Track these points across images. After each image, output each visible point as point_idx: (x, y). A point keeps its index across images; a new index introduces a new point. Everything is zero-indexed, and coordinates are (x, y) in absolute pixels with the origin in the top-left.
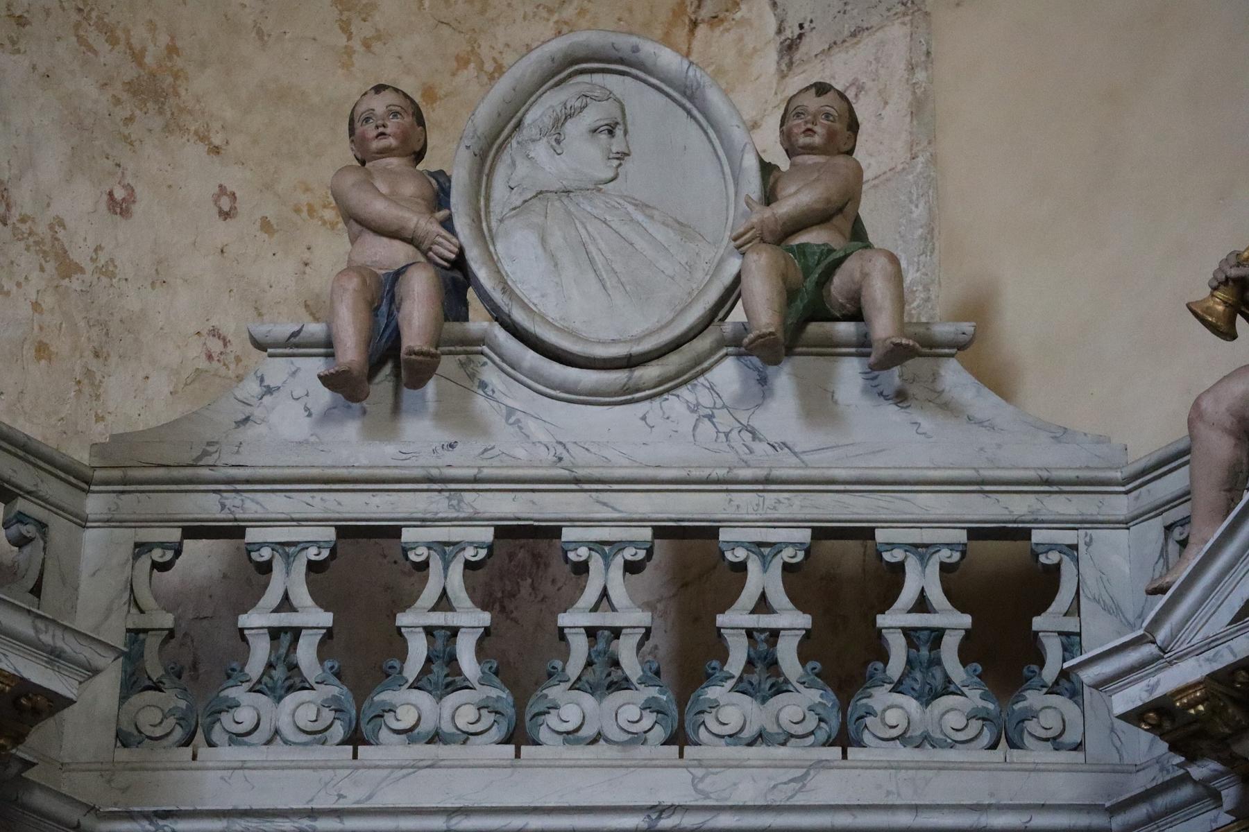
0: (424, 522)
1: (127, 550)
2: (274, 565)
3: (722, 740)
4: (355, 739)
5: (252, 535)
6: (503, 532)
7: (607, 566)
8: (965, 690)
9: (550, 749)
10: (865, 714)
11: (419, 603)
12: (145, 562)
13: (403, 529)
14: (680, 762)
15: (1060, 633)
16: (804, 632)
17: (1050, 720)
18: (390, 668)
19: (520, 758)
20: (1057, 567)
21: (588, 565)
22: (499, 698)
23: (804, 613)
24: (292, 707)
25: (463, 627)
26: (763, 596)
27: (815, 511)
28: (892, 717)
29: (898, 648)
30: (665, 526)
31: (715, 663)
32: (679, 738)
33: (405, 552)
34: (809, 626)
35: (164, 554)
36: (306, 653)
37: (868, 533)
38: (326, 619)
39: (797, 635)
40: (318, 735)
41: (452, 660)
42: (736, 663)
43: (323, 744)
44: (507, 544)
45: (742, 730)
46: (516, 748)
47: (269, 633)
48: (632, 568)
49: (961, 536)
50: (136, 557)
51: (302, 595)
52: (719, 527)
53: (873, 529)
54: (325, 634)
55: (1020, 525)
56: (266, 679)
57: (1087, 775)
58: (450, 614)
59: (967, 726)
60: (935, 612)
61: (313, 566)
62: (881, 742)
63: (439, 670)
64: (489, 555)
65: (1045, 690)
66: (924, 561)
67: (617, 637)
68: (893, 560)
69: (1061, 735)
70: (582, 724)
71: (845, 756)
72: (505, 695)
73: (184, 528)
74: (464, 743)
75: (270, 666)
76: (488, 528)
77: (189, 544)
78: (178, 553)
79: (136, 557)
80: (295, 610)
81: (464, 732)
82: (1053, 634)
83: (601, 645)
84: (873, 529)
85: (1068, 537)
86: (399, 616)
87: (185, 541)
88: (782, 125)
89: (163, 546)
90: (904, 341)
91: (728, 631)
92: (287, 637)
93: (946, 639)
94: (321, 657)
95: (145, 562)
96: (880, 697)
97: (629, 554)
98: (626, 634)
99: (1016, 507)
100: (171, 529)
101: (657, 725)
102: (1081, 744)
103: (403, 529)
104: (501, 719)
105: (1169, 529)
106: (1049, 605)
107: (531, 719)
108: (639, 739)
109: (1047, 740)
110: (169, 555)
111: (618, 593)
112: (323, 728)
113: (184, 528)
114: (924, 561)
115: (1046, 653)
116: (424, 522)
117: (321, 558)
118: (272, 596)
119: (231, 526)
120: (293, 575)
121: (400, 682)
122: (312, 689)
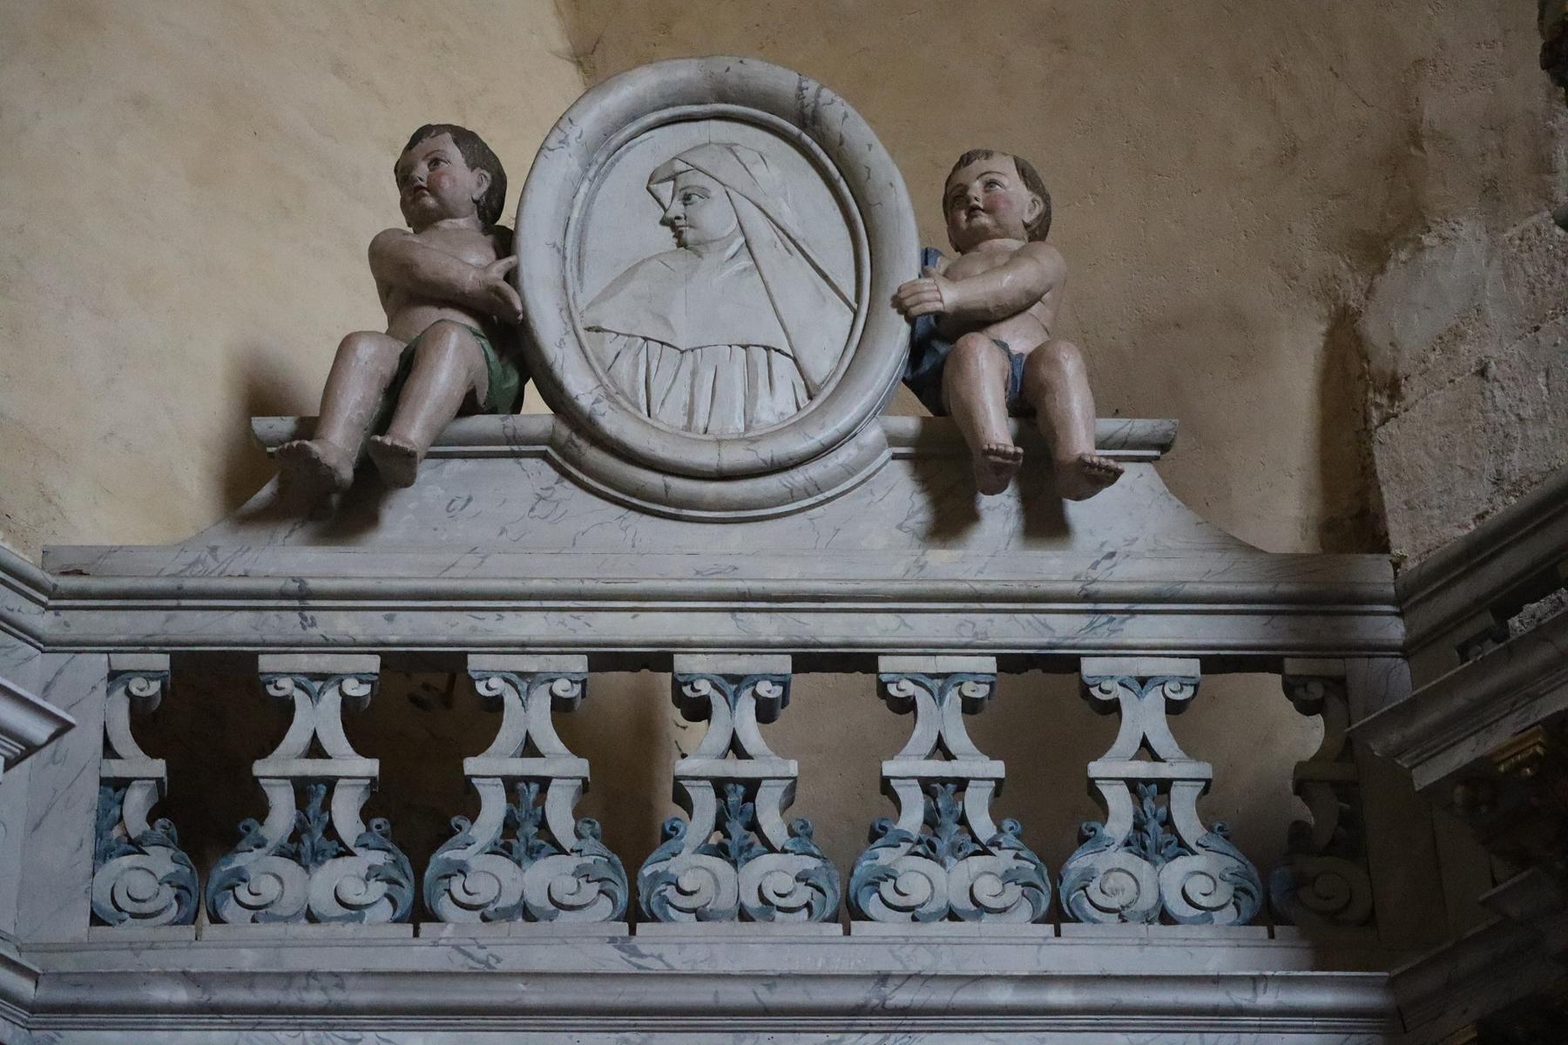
7: (732, 708)
14: (1057, 940)
19: (849, 934)
24: (1143, 884)
25: (135, 779)
26: (1145, 743)
29: (1119, 802)
31: (250, 822)
38: (998, 769)
39: (148, 785)
46: (630, 927)
47: (293, 784)
53: (1077, 658)
58: (319, 761)
59: (1003, 891)
60: (749, 757)
65: (905, 846)
66: (939, 697)
71: (847, 932)
73: (794, 655)
80: (540, 755)
82: (282, 781)
83: (1148, 804)
86: (1092, 765)
88: (947, 185)
91: (482, 780)
93: (762, 793)
100: (917, 658)
106: (489, 745)
112: (1217, 905)
114: (939, 697)
116: (707, 647)
119: (1249, 656)
120: (532, 711)
121: (1101, 844)
122: (351, 854)
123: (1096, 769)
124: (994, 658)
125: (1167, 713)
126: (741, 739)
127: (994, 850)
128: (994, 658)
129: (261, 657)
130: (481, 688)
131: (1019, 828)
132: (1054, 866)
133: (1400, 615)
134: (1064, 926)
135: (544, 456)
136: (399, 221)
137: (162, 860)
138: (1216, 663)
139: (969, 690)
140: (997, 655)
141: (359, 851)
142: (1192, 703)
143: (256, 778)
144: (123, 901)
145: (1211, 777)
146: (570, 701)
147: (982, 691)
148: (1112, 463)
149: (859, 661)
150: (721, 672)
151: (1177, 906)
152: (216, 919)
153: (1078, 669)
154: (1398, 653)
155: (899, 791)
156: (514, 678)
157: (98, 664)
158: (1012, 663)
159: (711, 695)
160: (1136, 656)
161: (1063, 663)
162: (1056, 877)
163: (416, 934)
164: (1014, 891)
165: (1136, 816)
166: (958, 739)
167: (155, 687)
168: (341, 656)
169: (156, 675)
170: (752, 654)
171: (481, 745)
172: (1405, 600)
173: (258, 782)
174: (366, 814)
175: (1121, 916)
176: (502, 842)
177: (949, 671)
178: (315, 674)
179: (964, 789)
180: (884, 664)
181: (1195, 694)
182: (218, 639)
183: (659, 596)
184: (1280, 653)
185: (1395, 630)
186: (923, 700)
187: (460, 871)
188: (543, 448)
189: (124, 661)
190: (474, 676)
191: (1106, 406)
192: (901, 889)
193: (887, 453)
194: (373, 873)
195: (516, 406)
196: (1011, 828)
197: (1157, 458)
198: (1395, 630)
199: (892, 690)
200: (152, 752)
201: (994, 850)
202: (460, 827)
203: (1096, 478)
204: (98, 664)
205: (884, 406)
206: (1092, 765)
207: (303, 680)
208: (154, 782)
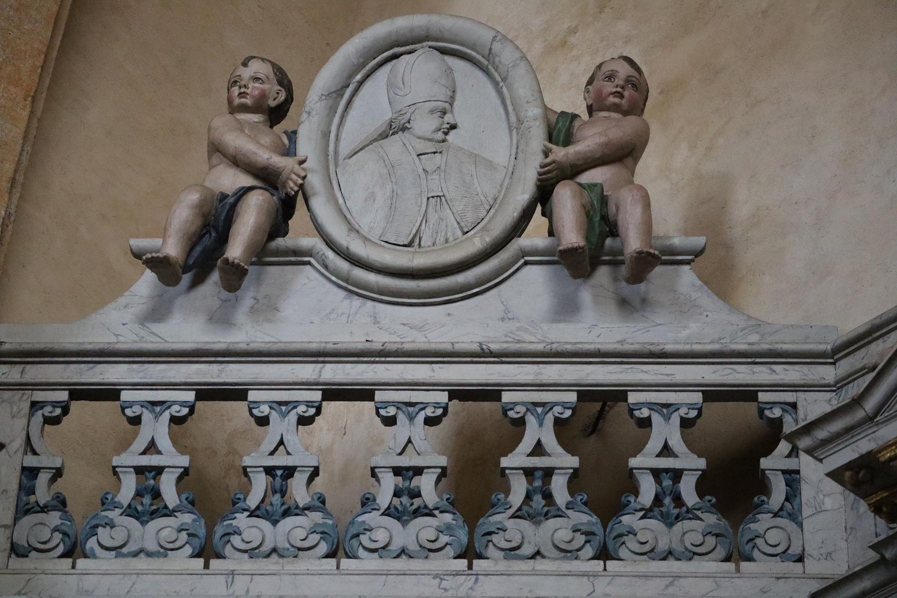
0: (136, 386)
1: (26, 406)
2: (142, 418)
3: (376, 555)
4: (470, 553)
9: (233, 562)
10: (233, 532)
11: (132, 448)
12: (38, 418)
15: (784, 472)
16: (183, 469)
20: (649, 419)
21: (141, 419)
22: (589, 523)
26: (539, 443)
28: (773, 536)
30: (224, 389)
32: (470, 553)
33: (631, 411)
36: (559, 486)
38: (573, 461)
39: (567, 473)
40: (567, 553)
43: (165, 557)
45: (260, 545)
46: (205, 563)
48: (430, 422)
50: (31, 414)
51: (164, 442)
53: (626, 392)
54: (55, 473)
55: (237, 387)
56: (525, 508)
58: (543, 458)
61: (176, 421)
62: (634, 555)
63: (538, 501)
65: (246, 514)
67: (291, 475)
68: (642, 416)
70: (789, 546)
72: (595, 519)
73: (450, 391)
74: (690, 559)
75: (528, 497)
76: (63, 392)
77: (75, 406)
78: (66, 410)
79: (31, 414)
81: (690, 551)
82: (518, 471)
84: (626, 392)
85: (789, 397)
86: (762, 460)
87: (197, 402)
89: (55, 404)
90: (652, 251)
94: (572, 492)
95: (38, 418)
97: (429, 412)
98: (686, 475)
101: (187, 545)
104: (67, 539)
107: (614, 538)
109: (245, 551)
110: (58, 411)
111: (292, 440)
113: (450, 391)
114: (667, 418)
115: (640, 486)
116: (136, 386)
118: (527, 443)
125: (681, 427)
127: (436, 512)
128: (447, 393)
129: (759, 394)
132: (471, 522)
134: (475, 562)
135: (526, 263)
141: (569, 512)
143: (763, 471)
145: (445, 465)
149: (237, 393)
150: (531, 401)
155: (380, 475)
156: (297, 404)
158: (586, 395)
164: (580, 539)
168: (785, 393)
171: (638, 448)
173: (764, 473)
177: (165, 400)
178: (281, 402)
180: (763, 397)
183: (625, 354)
186: (656, 419)
188: (522, 261)
189: (40, 396)
197: (693, 261)
201: (436, 512)
206: (762, 460)
207: (274, 405)
208: (54, 471)
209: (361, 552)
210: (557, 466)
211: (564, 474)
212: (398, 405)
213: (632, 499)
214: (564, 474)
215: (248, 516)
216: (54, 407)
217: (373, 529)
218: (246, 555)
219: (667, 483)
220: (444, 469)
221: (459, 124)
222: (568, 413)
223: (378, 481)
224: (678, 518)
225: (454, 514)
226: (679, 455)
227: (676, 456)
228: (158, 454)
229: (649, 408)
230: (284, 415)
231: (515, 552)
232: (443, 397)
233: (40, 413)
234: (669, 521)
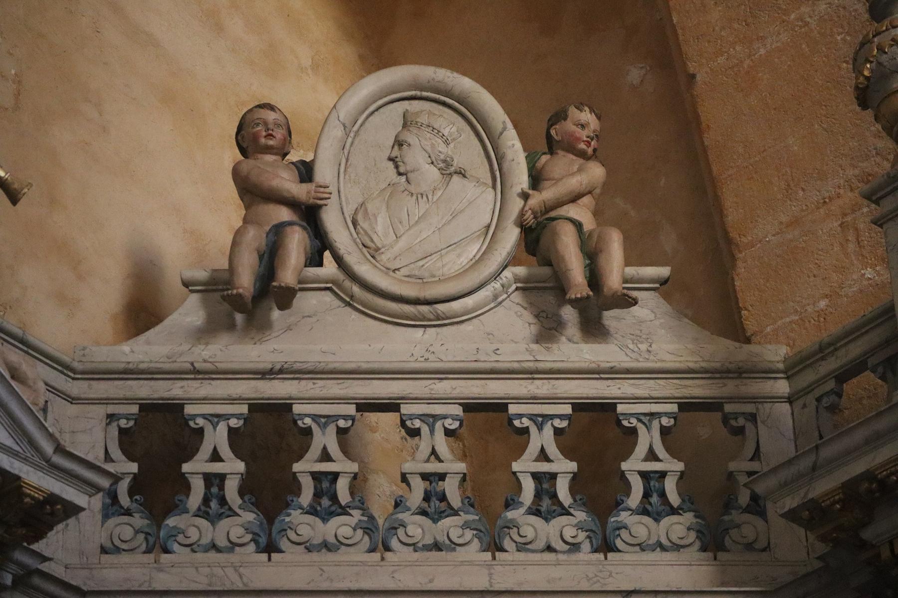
0: (311, 400)
5: (406, 409)
6: (578, 407)
8: (572, 511)
13: (185, 406)
17: (748, 532)
18: (179, 500)
19: (495, 559)
20: (419, 430)
23: (571, 461)
26: (543, 449)
27: (684, 390)
34: (576, 470)
35: (128, 423)
37: (503, 407)
39: (676, 475)
41: (554, 496)
42: (306, 497)
44: (585, 416)
45: (530, 542)
49: (674, 408)
52: (185, 404)
53: (615, 404)
57: (712, 567)
63: (546, 503)
64: (461, 425)
69: (199, 540)
71: (494, 558)
73: (250, 405)
76: (134, 406)
85: (749, 408)
89: (345, 417)
91: (522, 474)
92: (214, 481)
96: (295, 516)
99: (495, 389)
102: (766, 548)
103: (509, 405)
105: (819, 400)
108: (575, 547)
114: (540, 428)
117: (128, 426)
119: (389, 403)
123: (624, 466)
124: (570, 405)
126: (219, 450)
130: (191, 424)
131: (254, 500)
133: (788, 378)
134: (272, 555)
136: (240, 157)
137: (139, 521)
138: (686, 406)
139: (557, 423)
140: (356, 404)
142: (352, 428)
144: (117, 542)
145: (465, 472)
146: (670, 428)
147: (564, 424)
148: (625, 291)
149: (390, 406)
151: (558, 545)
152: (387, 548)
153: (507, 410)
154: (786, 400)
157: (101, 411)
158: (470, 407)
159: (312, 426)
160: (450, 403)
161: (499, 407)
162: (604, 524)
163: (270, 559)
165: (205, 494)
166: (552, 450)
167: (241, 422)
169: (349, 418)
170: (656, 403)
171: (627, 454)
172: (791, 370)
174: (242, 493)
175: (306, 548)
176: (534, 508)
179: (664, 477)
181: (352, 425)
182: (477, 396)
184: (721, 401)
185: (782, 387)
187: (403, 526)
190: (297, 417)
191: (628, 262)
192: (522, 534)
193: (514, 287)
194: (466, 525)
195: (320, 264)
196: (580, 499)
198: (782, 387)
199: (408, 423)
200: (131, 458)
202: (623, 501)
203: (626, 301)
204: (101, 411)
205: (513, 261)
209: (176, 547)
210: (227, 472)
211: (675, 475)
212: (423, 417)
213: (295, 499)
214: (675, 475)
215: (301, 513)
216: (128, 419)
217: (740, 525)
218: (188, 549)
219: (325, 485)
220: (465, 474)
221: (387, 158)
222: (131, 423)
223: (409, 485)
224: (220, 516)
225: (258, 515)
226: (225, 460)
227: (661, 461)
228: (656, 461)
229: (745, 419)
230: (323, 427)
231: (526, 546)
232: (351, 410)
233: (115, 424)
234: (212, 520)
